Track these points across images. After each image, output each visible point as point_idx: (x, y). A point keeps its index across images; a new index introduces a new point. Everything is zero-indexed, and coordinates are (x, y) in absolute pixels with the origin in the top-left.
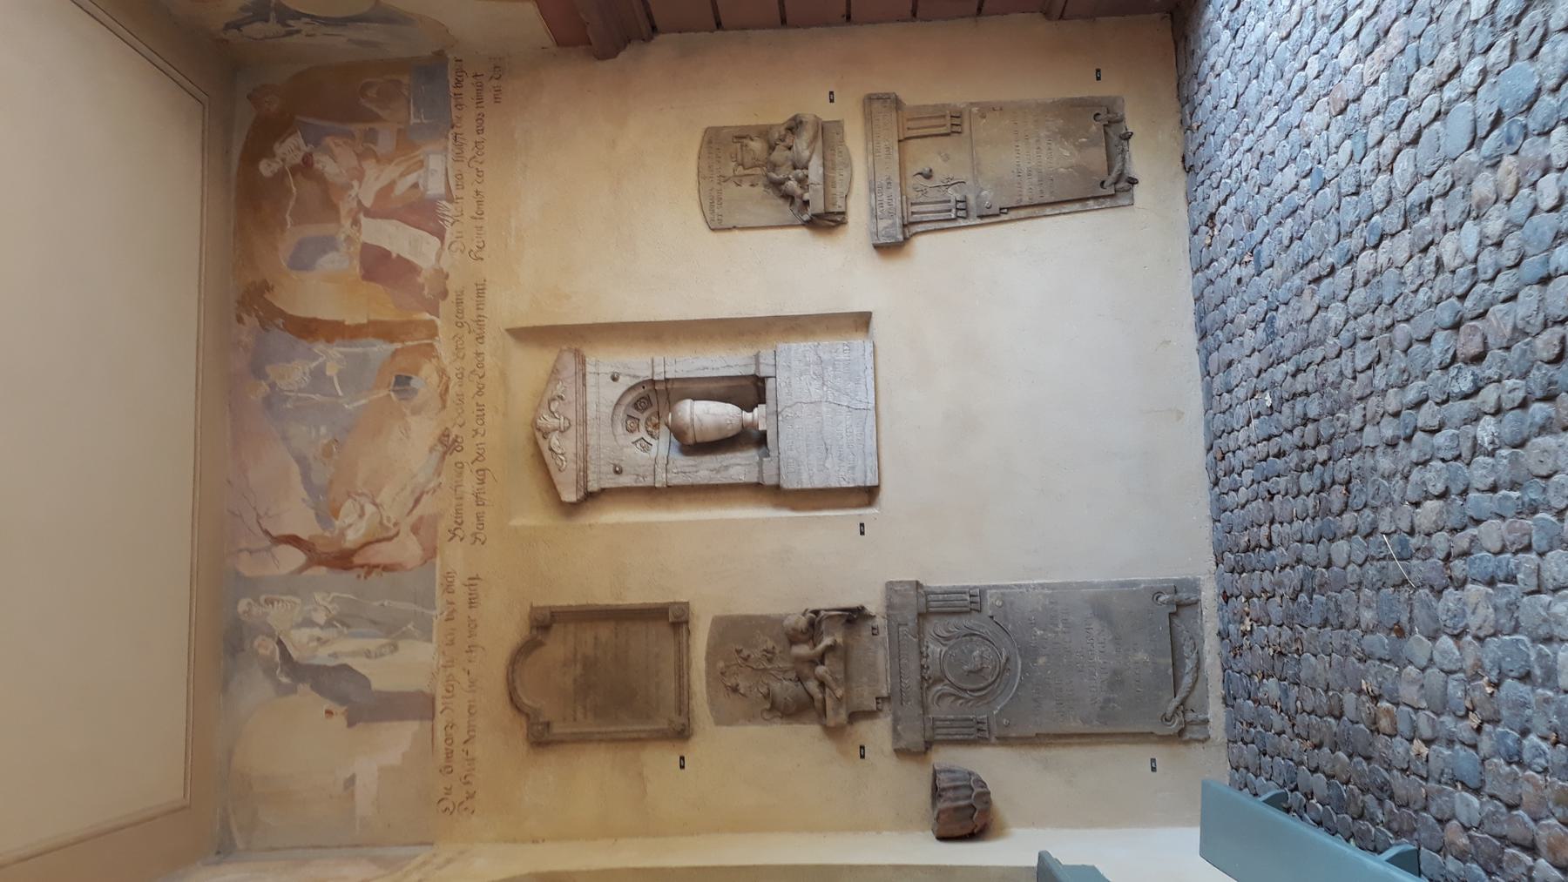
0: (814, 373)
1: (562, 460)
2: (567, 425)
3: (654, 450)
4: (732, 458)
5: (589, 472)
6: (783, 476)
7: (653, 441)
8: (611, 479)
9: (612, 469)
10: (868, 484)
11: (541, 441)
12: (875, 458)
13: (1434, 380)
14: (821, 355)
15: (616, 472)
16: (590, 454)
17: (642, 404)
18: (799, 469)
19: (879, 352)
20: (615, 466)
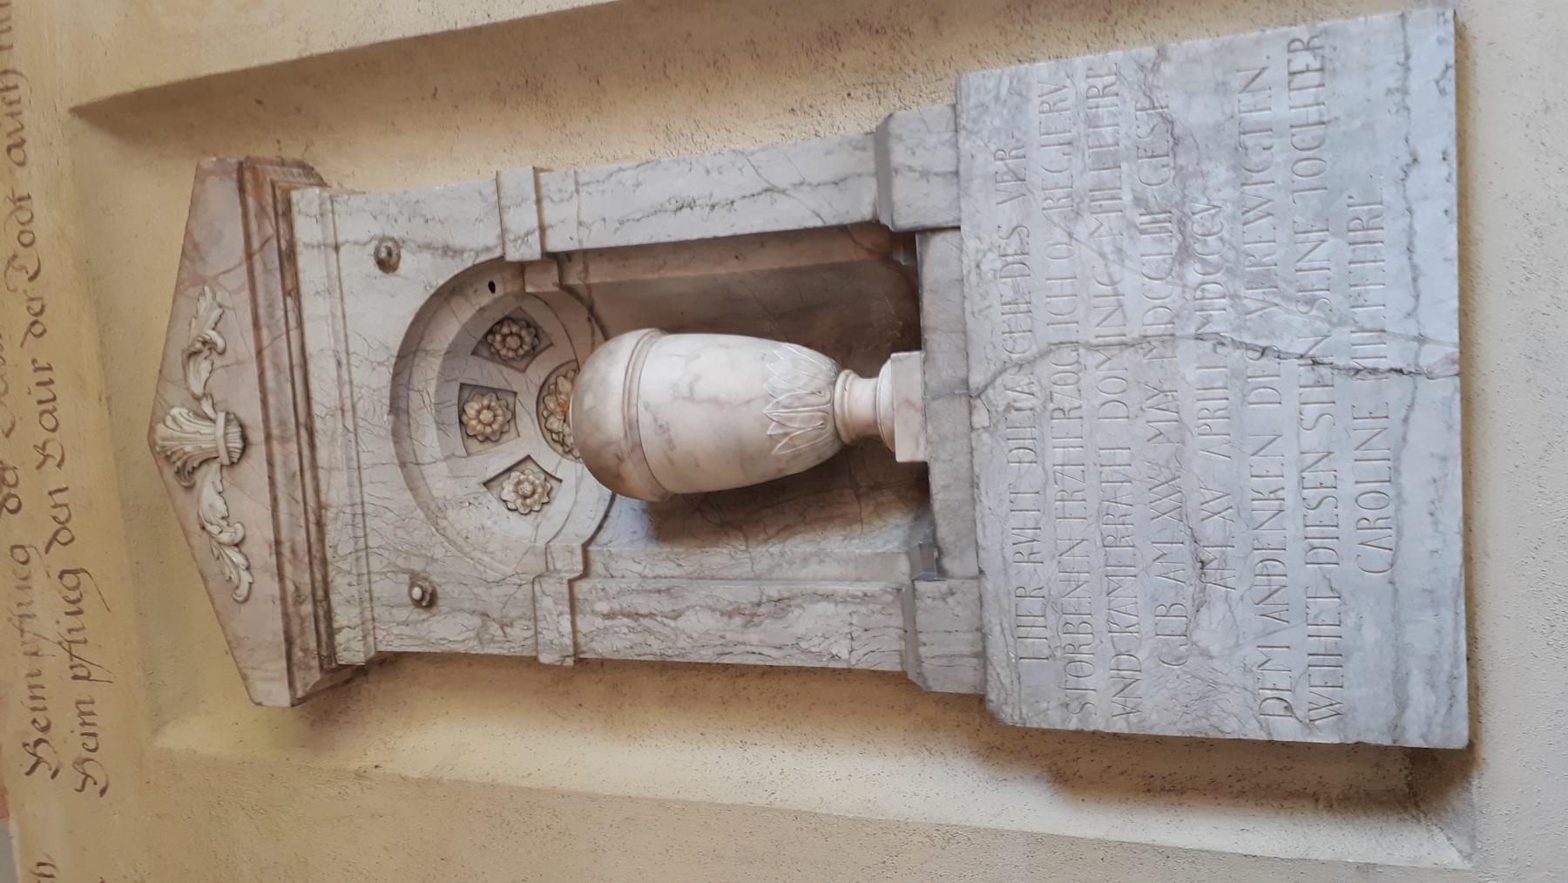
1: (236, 566)
4: (806, 560)
10: (1414, 739)
12: (1452, 618)
13: (679, 629)
14: (1176, 105)
17: (513, 342)
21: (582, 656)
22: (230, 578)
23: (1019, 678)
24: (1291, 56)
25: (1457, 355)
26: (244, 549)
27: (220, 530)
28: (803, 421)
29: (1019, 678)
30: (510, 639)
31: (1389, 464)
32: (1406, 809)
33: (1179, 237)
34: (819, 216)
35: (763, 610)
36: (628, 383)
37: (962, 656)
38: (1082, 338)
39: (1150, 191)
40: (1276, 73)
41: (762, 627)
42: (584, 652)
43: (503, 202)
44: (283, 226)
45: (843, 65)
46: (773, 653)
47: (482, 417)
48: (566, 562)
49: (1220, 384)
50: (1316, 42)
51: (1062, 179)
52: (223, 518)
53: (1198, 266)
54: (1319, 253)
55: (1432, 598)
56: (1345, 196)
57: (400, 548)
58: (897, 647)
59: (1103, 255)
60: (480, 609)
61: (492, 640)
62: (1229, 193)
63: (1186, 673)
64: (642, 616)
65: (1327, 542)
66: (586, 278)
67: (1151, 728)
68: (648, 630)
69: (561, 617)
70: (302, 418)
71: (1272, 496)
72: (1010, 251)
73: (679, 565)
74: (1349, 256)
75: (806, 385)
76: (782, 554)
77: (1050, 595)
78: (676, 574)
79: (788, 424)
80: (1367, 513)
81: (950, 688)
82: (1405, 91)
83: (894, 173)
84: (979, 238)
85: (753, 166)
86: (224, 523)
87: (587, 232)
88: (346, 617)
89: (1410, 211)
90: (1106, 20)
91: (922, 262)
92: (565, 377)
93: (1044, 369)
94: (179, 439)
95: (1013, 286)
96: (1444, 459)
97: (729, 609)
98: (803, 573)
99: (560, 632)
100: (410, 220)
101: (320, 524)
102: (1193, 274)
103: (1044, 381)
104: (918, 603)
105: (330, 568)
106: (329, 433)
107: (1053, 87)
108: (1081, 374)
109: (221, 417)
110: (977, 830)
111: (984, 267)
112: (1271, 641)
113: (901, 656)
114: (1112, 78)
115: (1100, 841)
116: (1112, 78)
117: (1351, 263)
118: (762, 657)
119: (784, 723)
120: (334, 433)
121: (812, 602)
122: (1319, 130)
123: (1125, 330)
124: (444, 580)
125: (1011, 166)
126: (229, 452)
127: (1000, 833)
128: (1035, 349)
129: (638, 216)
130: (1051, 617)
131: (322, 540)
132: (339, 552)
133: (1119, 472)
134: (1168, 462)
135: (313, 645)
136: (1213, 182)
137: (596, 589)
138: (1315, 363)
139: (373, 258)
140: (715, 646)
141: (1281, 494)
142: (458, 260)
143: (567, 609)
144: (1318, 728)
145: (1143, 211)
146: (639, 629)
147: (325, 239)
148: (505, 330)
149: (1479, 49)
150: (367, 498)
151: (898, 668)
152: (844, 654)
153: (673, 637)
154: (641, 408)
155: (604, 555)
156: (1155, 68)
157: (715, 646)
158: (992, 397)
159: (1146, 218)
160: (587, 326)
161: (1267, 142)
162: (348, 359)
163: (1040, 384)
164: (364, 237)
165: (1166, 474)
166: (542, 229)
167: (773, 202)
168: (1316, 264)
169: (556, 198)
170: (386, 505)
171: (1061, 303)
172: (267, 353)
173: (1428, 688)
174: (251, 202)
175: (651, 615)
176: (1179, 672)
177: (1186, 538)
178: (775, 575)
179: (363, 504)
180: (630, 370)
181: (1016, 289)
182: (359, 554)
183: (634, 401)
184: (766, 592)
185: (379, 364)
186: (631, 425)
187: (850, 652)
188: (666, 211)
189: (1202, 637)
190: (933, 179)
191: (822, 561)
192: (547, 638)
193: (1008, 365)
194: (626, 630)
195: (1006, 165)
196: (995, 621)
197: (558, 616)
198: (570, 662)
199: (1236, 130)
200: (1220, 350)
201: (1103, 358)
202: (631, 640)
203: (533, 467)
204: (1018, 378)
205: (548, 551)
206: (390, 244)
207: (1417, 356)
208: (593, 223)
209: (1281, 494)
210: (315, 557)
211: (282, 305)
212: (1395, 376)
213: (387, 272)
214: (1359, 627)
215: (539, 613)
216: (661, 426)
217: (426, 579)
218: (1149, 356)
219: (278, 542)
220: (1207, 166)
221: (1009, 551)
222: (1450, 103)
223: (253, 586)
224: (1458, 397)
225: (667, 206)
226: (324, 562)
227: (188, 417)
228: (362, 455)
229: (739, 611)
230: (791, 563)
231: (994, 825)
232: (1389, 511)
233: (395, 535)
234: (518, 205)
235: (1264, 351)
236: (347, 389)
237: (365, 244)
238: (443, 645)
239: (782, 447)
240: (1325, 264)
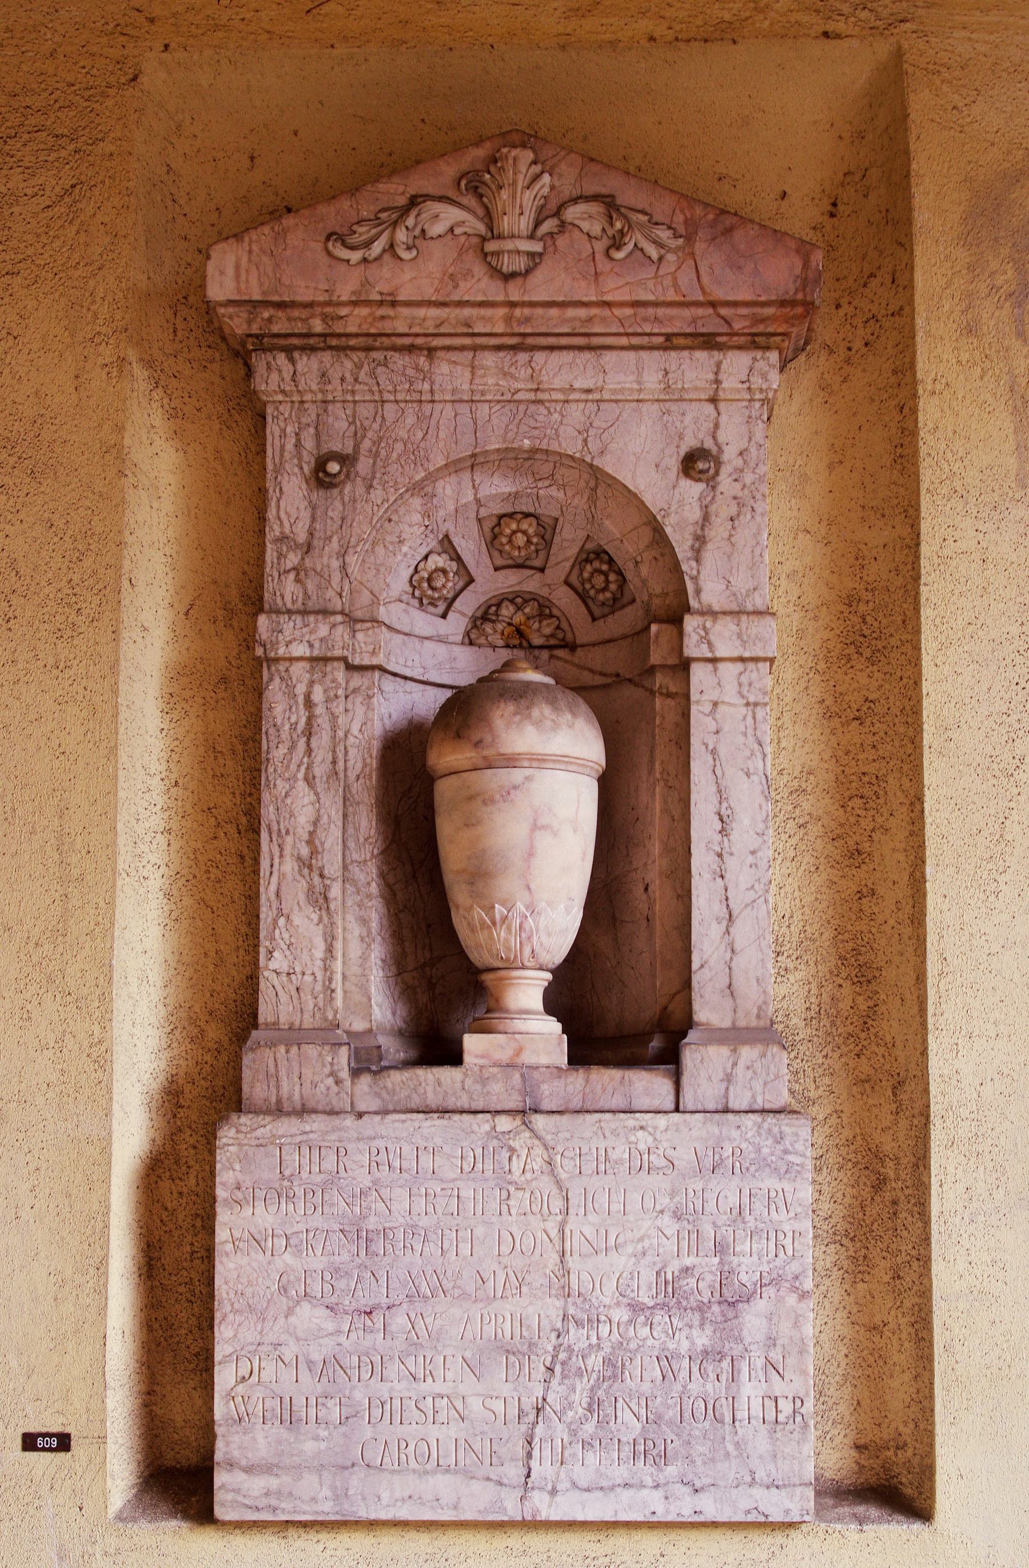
0: (686, 1270)
1: (368, 244)
2: (508, 264)
3: (423, 622)
4: (364, 922)
5: (327, 357)
6: (269, 1127)
7: (456, 624)
8: (298, 445)
9: (336, 447)
10: (220, 1478)
11: (449, 170)
12: (327, 1510)
13: (295, 782)
14: (760, 1305)
15: (321, 465)
16: (399, 361)
17: (599, 581)
18: (291, 1198)
19: (762, 1544)
20: (346, 460)
21: (265, 665)
22: (355, 233)
23: (261, 1145)
24: (791, 1398)
25: (538, 1518)
26: (387, 257)
27: (410, 227)
28: (507, 940)
29: (261, 1145)
30: (283, 577)
31: (453, 1466)
32: (147, 1467)
33: (651, 1304)
34: (702, 966)
35: (317, 880)
36: (553, 758)
37: (278, 1087)
38: (571, 1218)
39: (693, 1282)
40: (778, 1387)
41: (298, 877)
42: (269, 668)
43: (744, 618)
44: (742, 340)
45: (840, 986)
46: (273, 888)
47: (519, 535)
48: (363, 645)
49: (525, 1333)
50: (799, 1419)
51: (711, 1206)
52: (423, 231)
53: (625, 1318)
54: (629, 1416)
55: (340, 1495)
56: (674, 1437)
57: (382, 445)
58: (282, 1020)
59: (641, 1239)
60: (315, 542)
61: (281, 556)
62: (685, 1345)
63: (272, 1295)
64: (309, 739)
65: (387, 1415)
66: (661, 694)
67: (221, 1262)
68: (292, 748)
69: (307, 645)
70: (530, 341)
71: (428, 1372)
72: (652, 1158)
73: (358, 778)
74: (624, 1439)
75: (542, 944)
76: (369, 896)
77: (340, 1178)
78: (349, 773)
79: (504, 927)
80: (412, 1447)
81: (247, 1074)
82: (753, 1483)
83: (732, 1047)
84: (666, 1130)
85: (754, 901)
86: (417, 232)
87: (707, 712)
88: (306, 370)
89: (657, 1487)
90: (846, 1236)
91: (651, 1070)
92: (558, 627)
93: (545, 1184)
94: (514, 183)
95: (621, 1159)
96: (455, 1507)
97: (317, 842)
98: (350, 917)
99: (290, 642)
100: (735, 498)
101: (411, 349)
102: (621, 1315)
103: (534, 1183)
104: (327, 1048)
105: (362, 355)
106: (513, 370)
107: (789, 1201)
108: (539, 1216)
109: (537, 247)
110: (110, 1091)
111: (640, 1134)
112: (303, 1366)
113: (274, 1024)
114: (790, 1253)
115: (108, 1207)
116: (790, 1253)
117: (619, 1440)
118: (268, 873)
119: (191, 877)
120: (512, 376)
121: (325, 934)
122: (728, 1419)
123: (576, 1256)
124: (346, 499)
125: (726, 1162)
126: (498, 254)
127: (108, 1114)
128: (563, 1175)
129: (719, 772)
130: (319, 1179)
131: (394, 348)
132: (379, 368)
133: (451, 1245)
134: (459, 1287)
135: (276, 329)
136: (695, 1332)
137: (337, 688)
138: (538, 1410)
139: (699, 445)
140: (278, 823)
141: (429, 1379)
142: (690, 554)
143: (316, 653)
144: (228, 1402)
145: (676, 1274)
146: (295, 736)
147: (724, 390)
148: (612, 577)
149: (779, 1538)
150: (438, 407)
151: (261, 1019)
152: (273, 965)
153: (287, 775)
154: (527, 772)
155: (368, 688)
156: (794, 1289)
157: (278, 823)
158: (522, 1135)
159: (669, 1277)
160: (611, 669)
161: (723, 1378)
162: (592, 401)
163: (532, 1180)
164: (722, 438)
165: (447, 1285)
166: (714, 660)
167: (719, 921)
168: (619, 1414)
169: (744, 679)
170: (430, 432)
171: (603, 1200)
172: (606, 312)
173: (265, 1491)
174: (769, 311)
175: (309, 751)
176: (273, 1289)
177: (392, 1300)
178: (348, 886)
179: (433, 401)
180: (566, 759)
181: (619, 1162)
182: (377, 394)
183: (535, 764)
184: (335, 884)
185: (585, 441)
186: (511, 761)
187: (275, 971)
188: (720, 803)
189: (305, 1309)
190: (724, 1085)
191: (362, 939)
192: (285, 626)
193: (551, 1151)
194: (293, 719)
195: (728, 1157)
196: (315, 1126)
197: (308, 642)
198: (259, 652)
199: (735, 1353)
200: (554, 1335)
201: (552, 1236)
202: (283, 725)
203: (461, 584)
204: (539, 1160)
205: (375, 624)
206: (712, 472)
207: (541, 1489)
208: (715, 720)
209: (429, 1379)
210: (375, 341)
211: (656, 331)
212: (525, 1472)
213: (682, 462)
214: (316, 1438)
215: (312, 618)
216: (509, 793)
217: (348, 476)
218: (552, 1275)
219: (394, 304)
220: (709, 1329)
221: (381, 1144)
222: (740, 1517)
223: (345, 263)
224: (505, 1518)
225: (725, 805)
226: (368, 349)
227: (538, 198)
228: (486, 406)
229: (314, 852)
230: (360, 905)
231: (116, 1107)
232: (413, 1464)
233: (396, 440)
234: (739, 636)
235: (551, 1369)
236: (560, 396)
237: (714, 438)
238: (274, 491)
239: (478, 913)
240: (619, 1420)
